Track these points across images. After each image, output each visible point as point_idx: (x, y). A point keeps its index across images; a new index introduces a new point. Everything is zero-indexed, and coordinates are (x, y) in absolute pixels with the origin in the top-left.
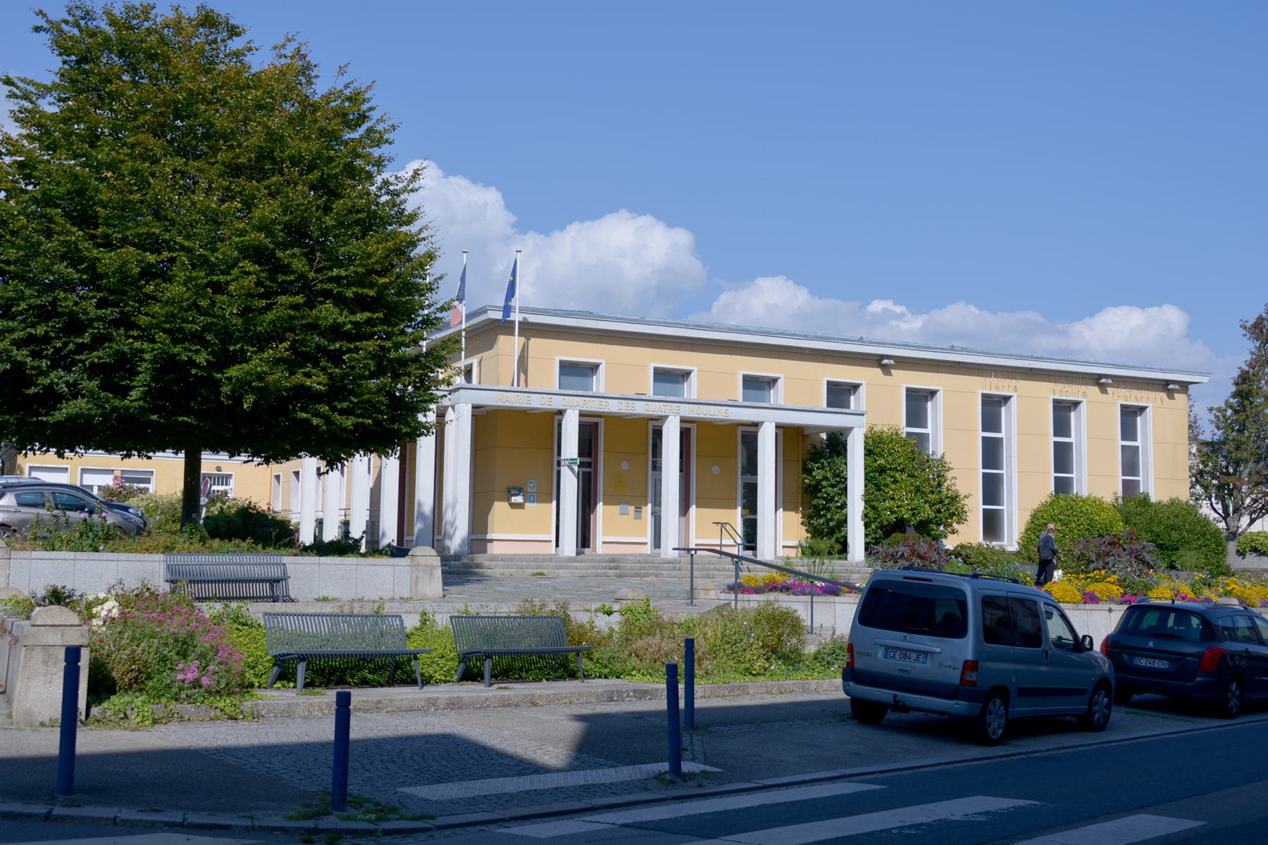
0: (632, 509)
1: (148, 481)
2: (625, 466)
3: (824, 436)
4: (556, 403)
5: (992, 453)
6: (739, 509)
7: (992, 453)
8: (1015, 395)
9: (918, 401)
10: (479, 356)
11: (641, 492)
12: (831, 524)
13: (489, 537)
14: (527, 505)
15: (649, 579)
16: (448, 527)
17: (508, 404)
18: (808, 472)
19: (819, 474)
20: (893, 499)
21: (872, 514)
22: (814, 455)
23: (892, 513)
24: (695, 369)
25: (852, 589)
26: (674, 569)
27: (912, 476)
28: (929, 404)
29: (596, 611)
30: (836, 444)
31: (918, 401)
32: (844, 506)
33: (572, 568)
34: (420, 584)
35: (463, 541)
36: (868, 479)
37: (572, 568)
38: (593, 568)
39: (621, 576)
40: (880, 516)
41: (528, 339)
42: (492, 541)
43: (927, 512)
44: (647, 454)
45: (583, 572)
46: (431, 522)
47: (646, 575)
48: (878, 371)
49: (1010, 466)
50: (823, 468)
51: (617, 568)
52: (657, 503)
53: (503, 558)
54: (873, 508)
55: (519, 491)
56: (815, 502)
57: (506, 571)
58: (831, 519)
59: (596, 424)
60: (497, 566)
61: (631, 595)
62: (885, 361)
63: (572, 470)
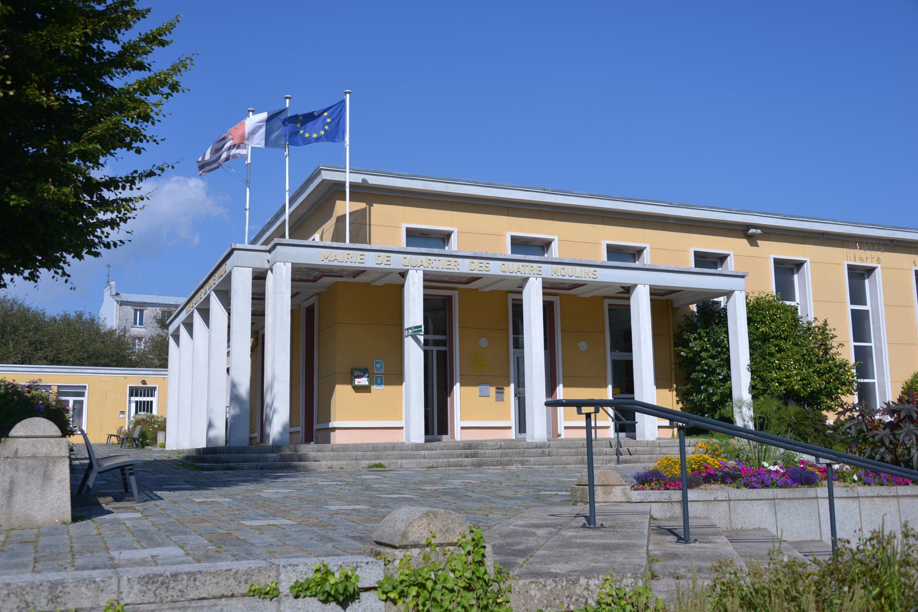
0: (493, 390)
1: (82, 395)
2: (484, 342)
3: (694, 308)
4: (397, 262)
5: (860, 322)
6: (610, 387)
7: (860, 322)
8: (879, 266)
9: (786, 270)
10: (320, 230)
11: (505, 371)
12: (715, 399)
13: (331, 425)
14: (374, 388)
15: (513, 468)
16: (268, 410)
17: (336, 263)
18: (686, 344)
19: (695, 345)
20: (780, 369)
21: (760, 386)
22: (689, 327)
23: (780, 384)
24: (556, 238)
25: (61, 457)
26: (543, 454)
27: (797, 345)
28: (796, 276)
29: (299, 591)
30: (712, 315)
31: (786, 270)
32: (728, 378)
33: (420, 457)
34: (19, 497)
35: (284, 428)
36: (752, 348)
37: (420, 457)
38: (445, 456)
39: (479, 465)
40: (769, 387)
41: (370, 205)
42: (334, 429)
43: (817, 383)
44: (507, 330)
45: (432, 462)
46: (247, 406)
47: (510, 463)
48: (744, 242)
49: (878, 338)
50: (701, 338)
51: (474, 455)
52: (520, 384)
53: (345, 448)
54: (763, 380)
55: (363, 372)
56: (694, 375)
57: (335, 463)
58: (713, 394)
59: (450, 298)
60: (324, 458)
61: (419, 533)
62: (752, 231)
63: (417, 341)
